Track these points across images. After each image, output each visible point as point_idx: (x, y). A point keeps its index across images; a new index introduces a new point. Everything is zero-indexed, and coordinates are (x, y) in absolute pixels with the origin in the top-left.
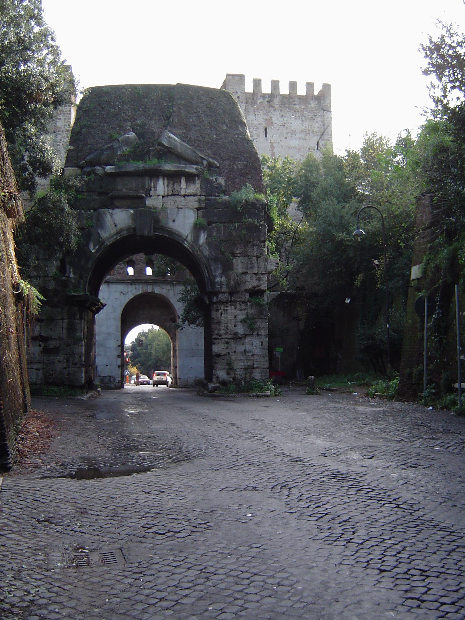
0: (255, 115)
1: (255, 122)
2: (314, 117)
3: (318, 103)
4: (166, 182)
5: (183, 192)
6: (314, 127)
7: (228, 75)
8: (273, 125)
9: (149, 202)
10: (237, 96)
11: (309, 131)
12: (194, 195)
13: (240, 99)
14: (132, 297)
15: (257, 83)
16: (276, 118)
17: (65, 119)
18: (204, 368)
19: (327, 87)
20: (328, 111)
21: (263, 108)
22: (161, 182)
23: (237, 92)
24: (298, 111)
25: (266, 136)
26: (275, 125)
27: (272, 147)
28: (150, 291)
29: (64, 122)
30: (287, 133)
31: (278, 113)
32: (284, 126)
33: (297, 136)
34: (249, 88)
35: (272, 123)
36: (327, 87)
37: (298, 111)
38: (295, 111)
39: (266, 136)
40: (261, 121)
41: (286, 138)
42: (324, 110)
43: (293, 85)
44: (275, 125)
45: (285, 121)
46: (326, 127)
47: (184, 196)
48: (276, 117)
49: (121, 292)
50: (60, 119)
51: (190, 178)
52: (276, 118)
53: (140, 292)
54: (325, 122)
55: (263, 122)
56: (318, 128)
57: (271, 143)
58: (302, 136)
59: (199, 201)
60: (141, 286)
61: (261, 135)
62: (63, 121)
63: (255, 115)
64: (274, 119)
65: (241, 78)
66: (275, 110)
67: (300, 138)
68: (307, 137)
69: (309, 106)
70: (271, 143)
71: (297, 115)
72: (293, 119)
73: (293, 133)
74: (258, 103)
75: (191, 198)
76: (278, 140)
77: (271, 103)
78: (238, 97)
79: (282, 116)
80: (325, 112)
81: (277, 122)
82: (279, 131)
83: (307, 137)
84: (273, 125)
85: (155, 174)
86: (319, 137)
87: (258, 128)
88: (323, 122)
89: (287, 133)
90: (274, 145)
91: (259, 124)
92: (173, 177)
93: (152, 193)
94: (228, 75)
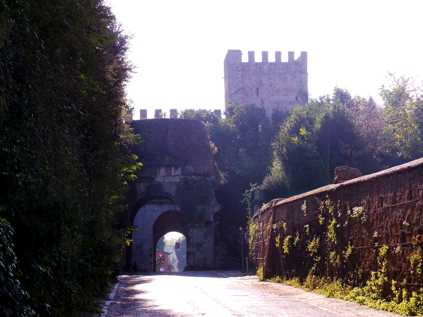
2: (294, 78)
3: (297, 68)
4: (164, 169)
6: (294, 86)
10: (235, 66)
12: (178, 176)
14: (161, 213)
19: (304, 55)
23: (235, 64)
24: (282, 75)
26: (264, 86)
28: (173, 209)
30: (273, 91)
32: (271, 86)
34: (245, 59)
35: (263, 84)
36: (304, 55)
39: (258, 94)
41: (273, 95)
42: (301, 73)
43: (278, 55)
44: (264, 86)
45: (272, 83)
46: (303, 85)
47: (173, 176)
49: (153, 210)
51: (176, 168)
53: (166, 210)
55: (255, 84)
57: (262, 99)
59: (180, 179)
60: (167, 206)
66: (264, 75)
67: (283, 95)
69: (290, 70)
70: (262, 99)
71: (281, 78)
73: (278, 91)
75: (177, 177)
77: (262, 70)
78: (237, 67)
79: (270, 79)
80: (302, 74)
85: (159, 166)
86: (297, 93)
87: (251, 89)
88: (301, 82)
89: (273, 91)
90: (264, 101)
91: (253, 86)
92: (168, 167)
93: (158, 174)
94: (229, 51)
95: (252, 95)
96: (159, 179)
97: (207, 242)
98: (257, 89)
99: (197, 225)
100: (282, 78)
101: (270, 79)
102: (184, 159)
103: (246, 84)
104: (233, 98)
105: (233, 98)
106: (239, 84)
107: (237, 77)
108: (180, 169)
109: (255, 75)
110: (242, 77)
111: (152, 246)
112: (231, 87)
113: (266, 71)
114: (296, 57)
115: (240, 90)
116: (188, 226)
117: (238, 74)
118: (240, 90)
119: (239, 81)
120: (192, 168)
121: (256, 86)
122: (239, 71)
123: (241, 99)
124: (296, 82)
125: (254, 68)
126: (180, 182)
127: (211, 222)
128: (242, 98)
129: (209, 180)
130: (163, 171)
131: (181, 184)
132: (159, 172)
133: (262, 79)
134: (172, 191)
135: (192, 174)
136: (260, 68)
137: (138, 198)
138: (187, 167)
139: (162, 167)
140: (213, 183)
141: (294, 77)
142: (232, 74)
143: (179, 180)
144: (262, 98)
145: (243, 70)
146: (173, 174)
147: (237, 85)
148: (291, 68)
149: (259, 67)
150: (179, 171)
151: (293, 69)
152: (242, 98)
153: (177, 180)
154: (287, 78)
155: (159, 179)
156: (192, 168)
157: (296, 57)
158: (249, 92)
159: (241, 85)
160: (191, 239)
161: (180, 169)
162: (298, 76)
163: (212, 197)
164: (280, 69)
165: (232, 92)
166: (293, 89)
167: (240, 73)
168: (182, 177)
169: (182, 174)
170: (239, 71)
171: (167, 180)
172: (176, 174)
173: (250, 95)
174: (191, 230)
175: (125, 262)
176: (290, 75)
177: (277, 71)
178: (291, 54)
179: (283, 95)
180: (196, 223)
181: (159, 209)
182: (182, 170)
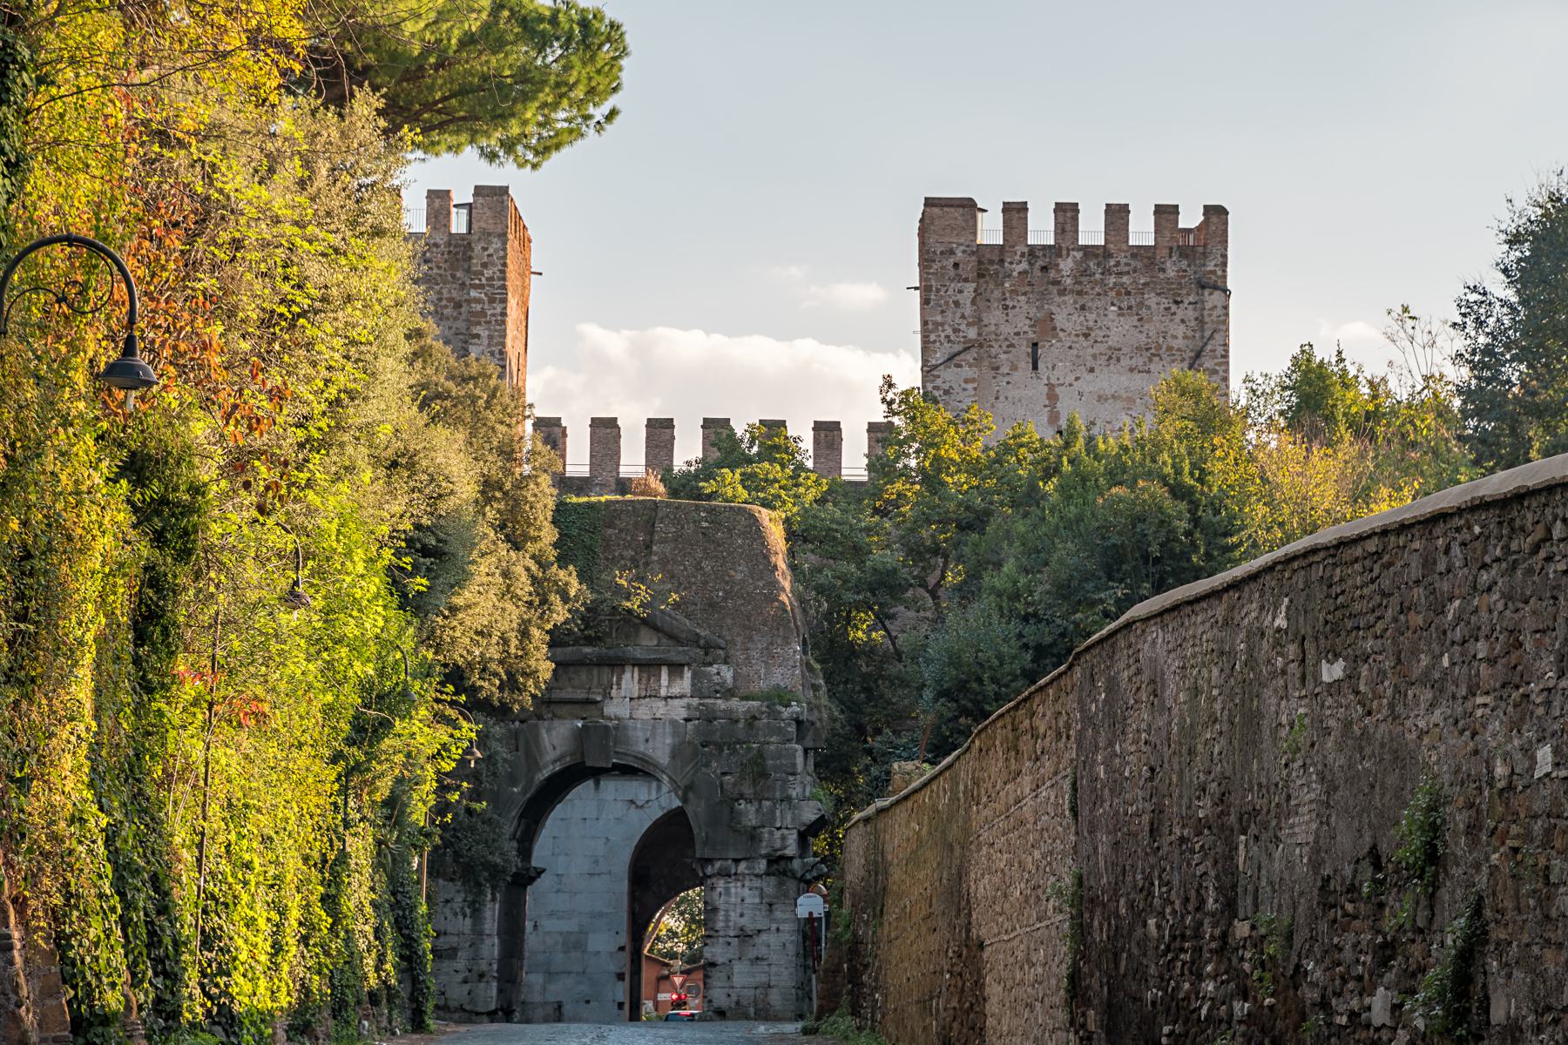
0: (1006, 307)
1: (1006, 330)
2: (1174, 307)
3: (1186, 264)
5: (663, 692)
6: (1175, 337)
7: (929, 202)
8: (1056, 336)
9: (611, 709)
10: (952, 261)
11: (1159, 347)
13: (960, 271)
15: (1015, 213)
16: (1066, 316)
17: (490, 337)
18: (624, 887)
19: (1216, 214)
20: (1215, 288)
21: (1028, 289)
22: (627, 676)
23: (952, 252)
24: (1128, 293)
25: (1035, 367)
26: (1061, 334)
27: (1053, 397)
29: (489, 345)
30: (1094, 357)
31: (1069, 299)
32: (1086, 336)
33: (1125, 362)
35: (1054, 328)
37: (1128, 293)
38: (1119, 293)
39: (1035, 367)
40: (1023, 325)
41: (1092, 370)
44: (1061, 334)
45: (1091, 324)
47: (666, 698)
48: (1066, 311)
49: (632, 802)
50: (478, 336)
51: (676, 668)
52: (1066, 316)
54: (1207, 319)
55: (1026, 328)
56: (1185, 337)
58: (1139, 361)
59: (688, 707)
61: (1022, 365)
62: (486, 342)
63: (1006, 307)
64: (1060, 320)
65: (968, 207)
66: (1062, 293)
68: (1152, 367)
69: (1161, 276)
70: (1051, 386)
71: (1125, 305)
72: (1111, 316)
74: (1015, 274)
76: (1071, 378)
77: (1052, 274)
78: (956, 265)
79: (1083, 308)
80: (1206, 292)
81: (1068, 326)
82: (1075, 352)
83: (1152, 367)
84: (1056, 336)
85: (617, 664)
87: (1012, 345)
89: (1094, 357)
90: (1058, 390)
91: (1017, 334)
92: (649, 667)
93: (614, 693)
95: (1014, 368)
96: (616, 708)
97: (774, 926)
98: (1035, 345)
99: (742, 867)
100: (1130, 308)
101: (1083, 308)
102: (702, 642)
103: (993, 328)
104: (939, 382)
105: (939, 382)
106: (963, 327)
107: (957, 304)
108: (688, 674)
109: (1025, 294)
110: (973, 302)
111: (624, 939)
112: (933, 337)
113: (1069, 281)
114: (1190, 219)
115: (965, 349)
116: (709, 870)
117: (960, 292)
118: (965, 349)
119: (963, 317)
120: (728, 674)
121: (1031, 335)
122: (966, 280)
123: (970, 386)
124: (1183, 321)
125: (1024, 266)
126: (687, 720)
127: (791, 859)
128: (973, 380)
129: (786, 713)
130: (630, 682)
131: (690, 725)
132: (619, 684)
133: (1054, 309)
134: (660, 750)
135: (729, 693)
136: (1044, 269)
137: (546, 773)
138: (713, 669)
139: (628, 669)
140: (799, 723)
141: (1177, 303)
142: (938, 290)
143: (684, 713)
144: (1054, 381)
145: (981, 276)
146: (663, 692)
147: (956, 331)
148: (1164, 270)
149: (1040, 263)
150: (685, 683)
151: (1171, 273)
152: (973, 380)
153: (678, 710)
154: (1149, 308)
155: (616, 708)
156: (728, 674)
157: (1190, 219)
158: (1003, 356)
159: (972, 333)
160: (721, 915)
161: (688, 674)
162: (1191, 299)
163: (794, 774)
164: (1120, 274)
165: (939, 357)
166: (1170, 348)
167: (971, 286)
168: (695, 701)
169: (696, 692)
170: (974, 272)
171: (644, 712)
172: (676, 690)
173: (1005, 370)
174: (721, 884)
175: (494, 992)
176: (1158, 294)
177: (1112, 280)
178: (1167, 214)
179: (1131, 370)
180: (737, 861)
181: (654, 796)
182: (695, 676)
